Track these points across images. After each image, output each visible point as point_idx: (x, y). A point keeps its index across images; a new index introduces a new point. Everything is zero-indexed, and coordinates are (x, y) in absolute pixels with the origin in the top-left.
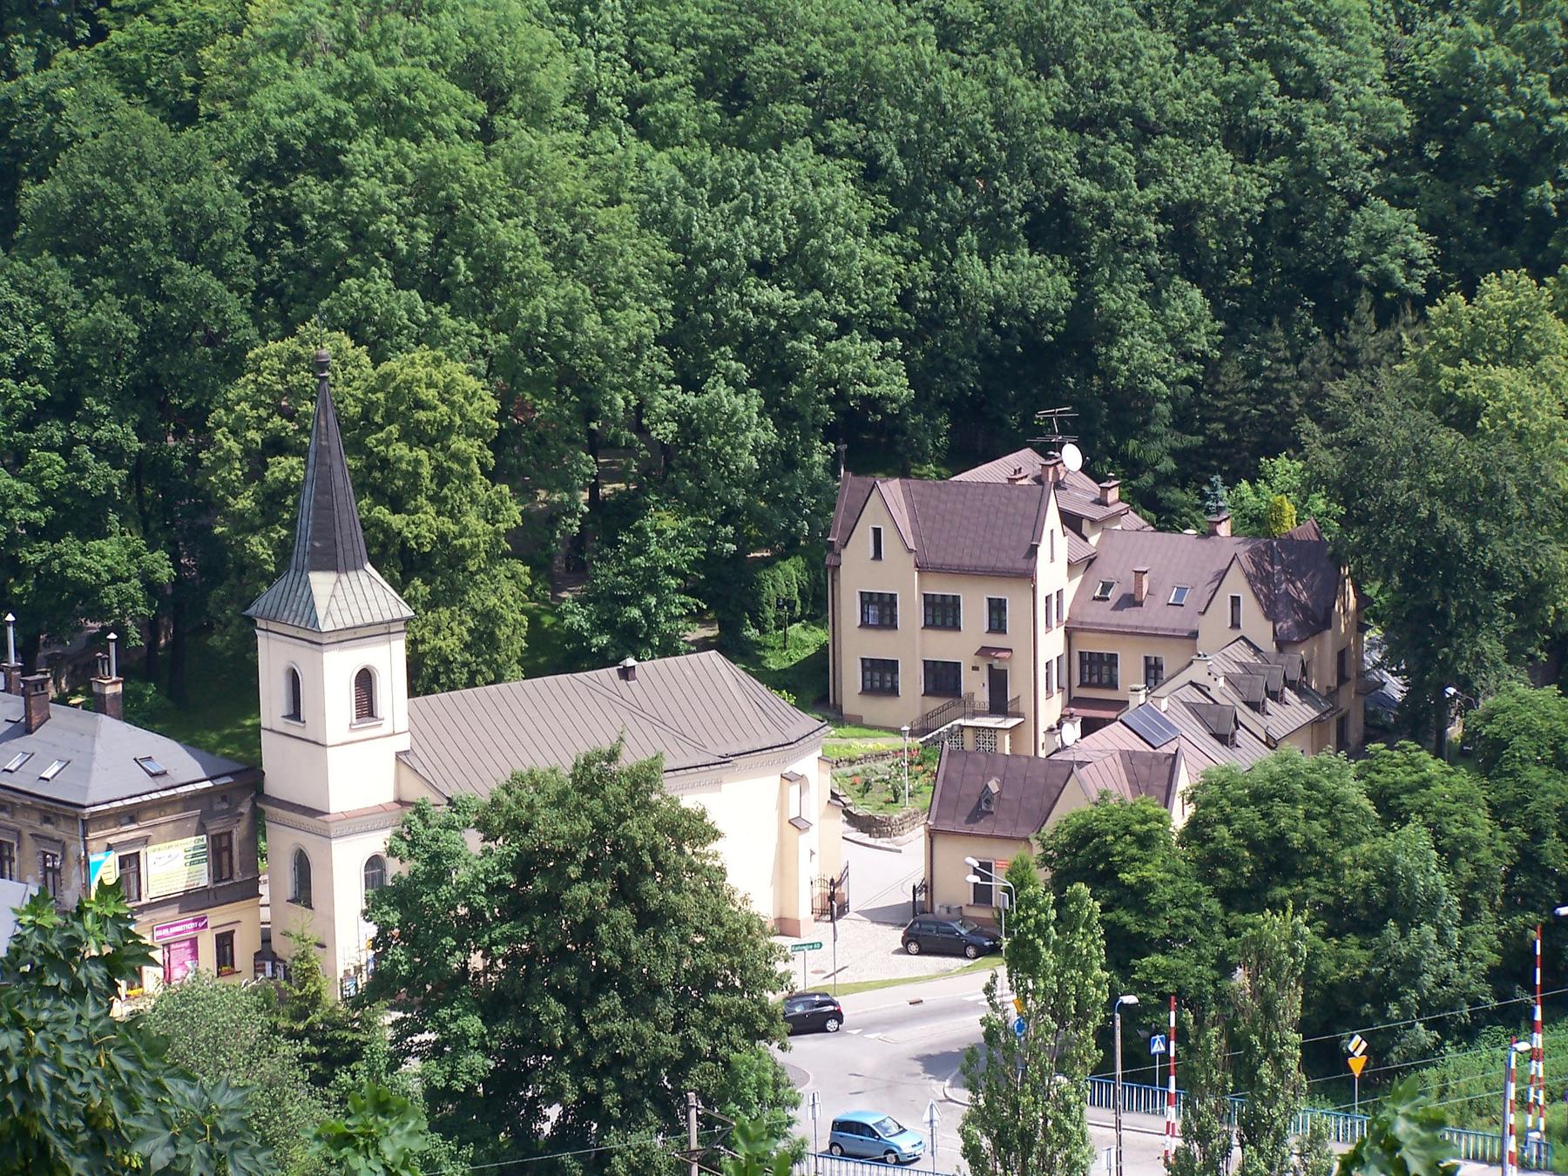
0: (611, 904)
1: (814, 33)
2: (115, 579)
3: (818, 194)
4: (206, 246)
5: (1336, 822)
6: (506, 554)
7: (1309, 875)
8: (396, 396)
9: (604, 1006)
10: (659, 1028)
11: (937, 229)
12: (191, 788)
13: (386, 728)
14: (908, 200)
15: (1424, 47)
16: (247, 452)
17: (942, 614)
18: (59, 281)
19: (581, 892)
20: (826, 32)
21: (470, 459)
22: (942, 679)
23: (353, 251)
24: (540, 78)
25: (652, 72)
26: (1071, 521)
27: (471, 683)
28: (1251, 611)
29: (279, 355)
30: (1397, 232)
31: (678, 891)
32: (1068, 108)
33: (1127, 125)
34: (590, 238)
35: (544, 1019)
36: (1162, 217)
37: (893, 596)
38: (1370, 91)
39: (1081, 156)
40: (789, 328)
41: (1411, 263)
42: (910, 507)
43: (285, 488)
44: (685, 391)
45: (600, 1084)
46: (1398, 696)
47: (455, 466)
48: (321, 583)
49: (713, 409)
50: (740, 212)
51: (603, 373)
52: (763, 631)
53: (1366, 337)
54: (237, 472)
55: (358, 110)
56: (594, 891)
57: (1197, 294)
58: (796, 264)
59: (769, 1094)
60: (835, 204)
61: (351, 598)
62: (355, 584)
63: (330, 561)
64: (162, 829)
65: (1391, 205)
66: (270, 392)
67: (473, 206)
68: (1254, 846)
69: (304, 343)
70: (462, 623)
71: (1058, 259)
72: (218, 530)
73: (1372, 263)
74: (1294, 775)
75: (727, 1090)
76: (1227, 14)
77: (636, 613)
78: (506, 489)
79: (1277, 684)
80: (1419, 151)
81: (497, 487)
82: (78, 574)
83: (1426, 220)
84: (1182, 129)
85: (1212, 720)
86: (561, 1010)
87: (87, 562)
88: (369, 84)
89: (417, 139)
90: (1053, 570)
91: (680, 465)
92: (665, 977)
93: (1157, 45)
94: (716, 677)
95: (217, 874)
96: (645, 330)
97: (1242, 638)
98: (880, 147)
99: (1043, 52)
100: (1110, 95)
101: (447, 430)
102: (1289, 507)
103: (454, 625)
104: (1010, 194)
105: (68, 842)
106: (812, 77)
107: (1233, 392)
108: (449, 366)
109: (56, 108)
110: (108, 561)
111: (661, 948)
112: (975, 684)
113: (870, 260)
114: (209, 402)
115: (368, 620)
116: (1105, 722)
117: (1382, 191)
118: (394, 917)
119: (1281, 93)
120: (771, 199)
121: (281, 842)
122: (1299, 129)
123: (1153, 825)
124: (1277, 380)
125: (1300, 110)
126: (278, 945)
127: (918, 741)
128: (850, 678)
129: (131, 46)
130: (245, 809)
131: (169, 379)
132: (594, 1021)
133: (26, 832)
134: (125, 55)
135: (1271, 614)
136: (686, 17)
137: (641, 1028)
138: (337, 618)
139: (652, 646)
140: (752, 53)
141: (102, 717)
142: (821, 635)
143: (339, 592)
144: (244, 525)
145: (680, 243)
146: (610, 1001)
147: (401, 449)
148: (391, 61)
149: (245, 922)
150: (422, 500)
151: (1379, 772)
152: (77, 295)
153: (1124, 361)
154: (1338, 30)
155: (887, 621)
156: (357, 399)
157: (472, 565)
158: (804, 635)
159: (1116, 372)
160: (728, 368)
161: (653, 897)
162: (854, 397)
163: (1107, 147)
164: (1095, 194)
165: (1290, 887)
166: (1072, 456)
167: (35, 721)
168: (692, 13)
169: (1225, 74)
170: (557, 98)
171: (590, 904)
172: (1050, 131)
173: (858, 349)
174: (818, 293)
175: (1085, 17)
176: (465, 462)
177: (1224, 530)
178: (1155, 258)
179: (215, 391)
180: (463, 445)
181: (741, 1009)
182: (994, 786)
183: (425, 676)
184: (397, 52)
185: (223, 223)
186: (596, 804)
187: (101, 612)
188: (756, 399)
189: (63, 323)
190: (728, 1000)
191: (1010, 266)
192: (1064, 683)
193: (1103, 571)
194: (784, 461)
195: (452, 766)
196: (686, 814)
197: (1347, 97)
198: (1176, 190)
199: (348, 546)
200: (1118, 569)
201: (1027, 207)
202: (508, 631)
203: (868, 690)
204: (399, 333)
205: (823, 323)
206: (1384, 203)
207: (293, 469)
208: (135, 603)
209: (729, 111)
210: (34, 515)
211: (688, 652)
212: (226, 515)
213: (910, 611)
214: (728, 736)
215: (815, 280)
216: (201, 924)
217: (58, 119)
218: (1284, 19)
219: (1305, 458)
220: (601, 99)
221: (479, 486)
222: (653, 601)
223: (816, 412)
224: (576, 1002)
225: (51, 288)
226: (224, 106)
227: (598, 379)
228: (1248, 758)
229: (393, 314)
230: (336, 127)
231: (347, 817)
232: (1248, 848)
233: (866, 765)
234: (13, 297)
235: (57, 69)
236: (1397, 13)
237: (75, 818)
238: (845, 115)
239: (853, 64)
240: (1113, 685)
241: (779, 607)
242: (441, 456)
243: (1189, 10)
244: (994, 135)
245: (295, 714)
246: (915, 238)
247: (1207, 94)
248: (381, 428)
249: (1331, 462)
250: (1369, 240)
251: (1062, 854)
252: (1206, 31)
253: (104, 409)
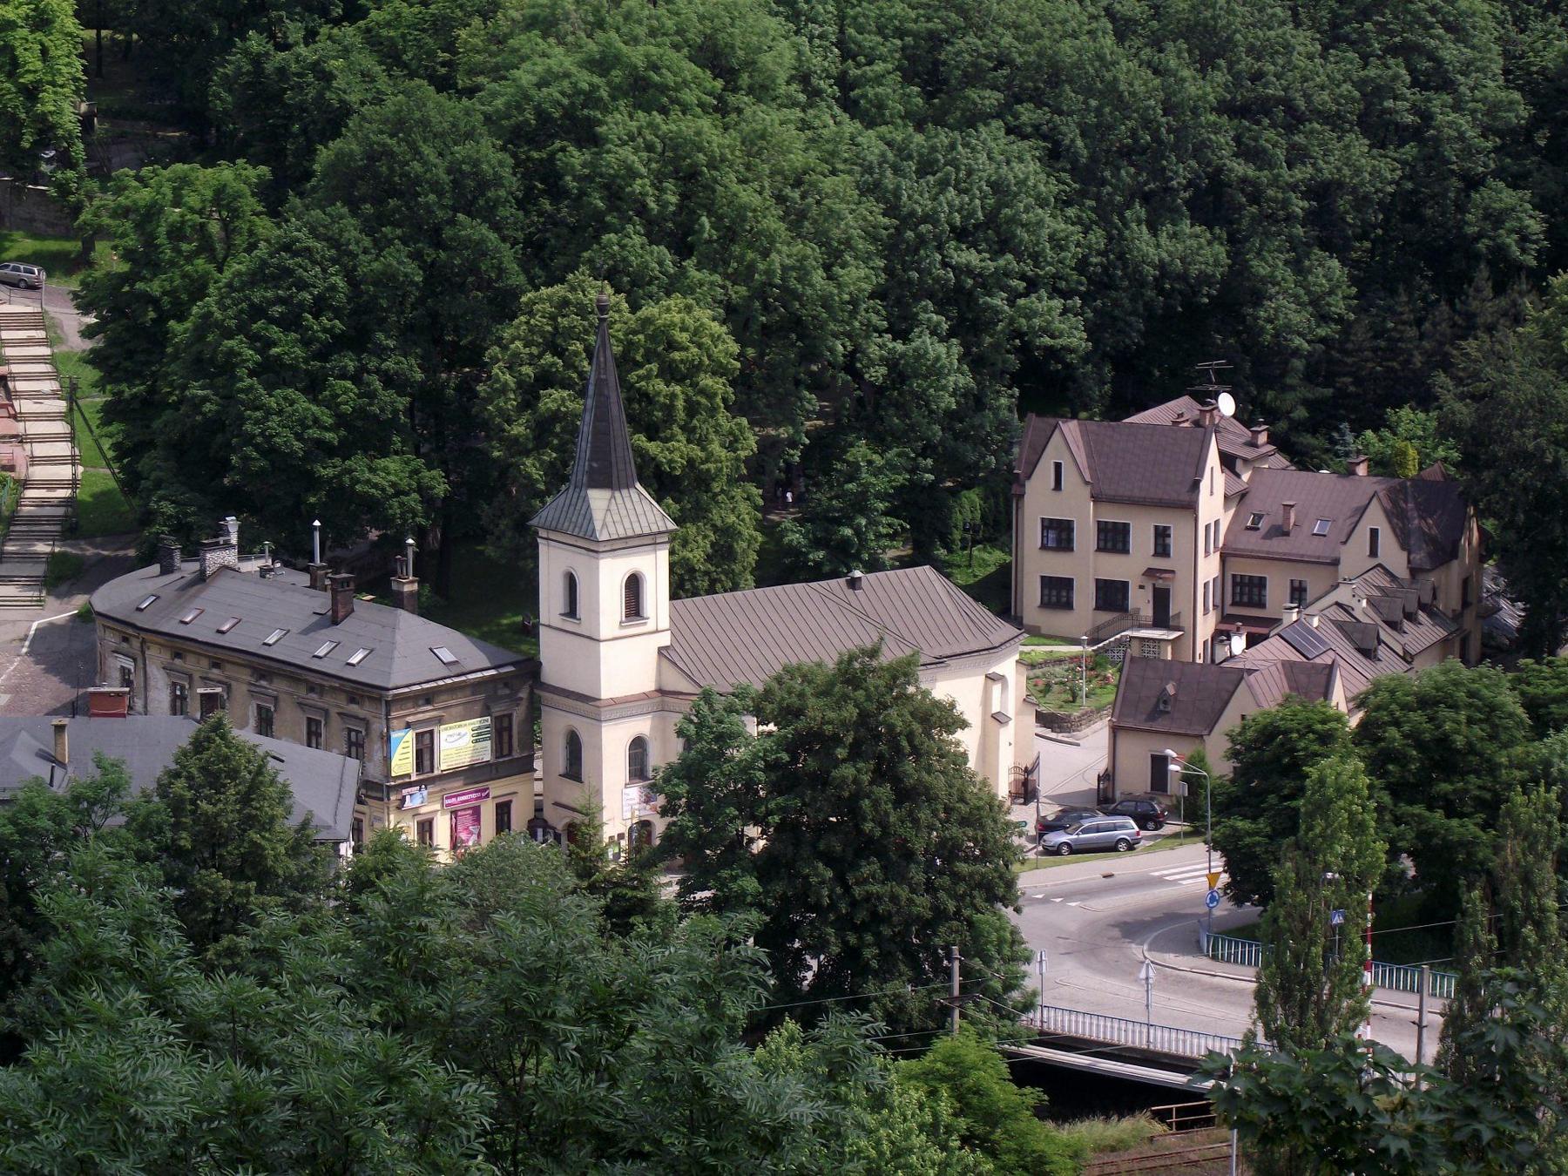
0: (871, 783)
1: (1006, 26)
2: (398, 493)
3: (1012, 169)
4: (481, 202)
5: (1494, 726)
6: (742, 478)
7: (1469, 773)
8: (652, 338)
9: (865, 871)
10: (913, 891)
11: (1111, 201)
12: (479, 675)
13: (651, 626)
14: (1087, 176)
15: (1539, 45)
16: (520, 384)
18: (351, 230)
19: (848, 771)
20: (1017, 26)
21: (716, 394)
22: (1111, 595)
23: (610, 210)
24: (766, 59)
25: (862, 59)
26: (1228, 461)
27: (711, 591)
28: (1387, 540)
29: (549, 299)
30: (1513, 210)
31: (929, 771)
32: (1229, 97)
33: (1279, 112)
34: (818, 203)
35: (813, 880)
36: (1305, 196)
38: (1491, 84)
39: (1238, 139)
40: (983, 286)
41: (1524, 238)
42: (1087, 444)
43: (555, 416)
44: (894, 340)
45: (860, 938)
46: (1513, 622)
47: (703, 401)
48: (598, 499)
49: (920, 355)
50: (943, 184)
51: (826, 322)
52: (950, 551)
53: (1484, 303)
54: (511, 402)
55: (609, 84)
56: (859, 771)
57: (1335, 263)
58: (994, 231)
59: (1006, 951)
60: (1027, 178)
61: (623, 512)
62: (627, 500)
63: (605, 479)
64: (453, 711)
65: (1508, 186)
66: (542, 334)
67: (715, 173)
68: (1420, 745)
69: (573, 289)
70: (705, 537)
71: (1217, 231)
72: (496, 454)
73: (1490, 238)
74: (1456, 684)
75: (976, 947)
76: (1365, 15)
77: (848, 532)
78: (744, 421)
79: (1412, 606)
80: (1529, 139)
81: (738, 420)
82: (366, 488)
83: (1537, 200)
84: (1333, 120)
85: (1356, 636)
86: (829, 874)
87: (376, 479)
88: (617, 59)
89: (664, 111)
90: (1212, 504)
91: (878, 407)
92: (919, 846)
93: (1304, 41)
94: (930, 589)
95: (499, 750)
96: (864, 286)
97: (1380, 565)
98: (1064, 129)
99: (1209, 47)
100: (1266, 86)
101: (696, 368)
102: (1412, 452)
103: (699, 539)
104: (1176, 173)
105: (372, 720)
106: (1000, 64)
107: (1361, 350)
108: (697, 312)
109: (327, 77)
110: (392, 478)
111: (916, 821)
112: (1140, 601)
113: (1055, 229)
114: (484, 339)
115: (638, 531)
116: (1266, 637)
117: (1498, 174)
118: (683, 789)
119: (1413, 85)
120: (970, 173)
121: (555, 725)
122: (1427, 117)
123: (1333, 725)
124: (1400, 340)
125: (1429, 100)
126: (550, 814)
127: (1090, 649)
128: (1031, 593)
129: (388, 24)
130: (524, 694)
131: (449, 319)
132: (857, 883)
133: (333, 711)
134: (384, 32)
135: (1405, 545)
136: (893, 12)
137: (897, 889)
138: (612, 530)
139: (861, 561)
140: (952, 44)
141: (401, 611)
142: (994, 557)
143: (613, 507)
144: (516, 447)
145: (892, 210)
146: (871, 867)
147: (660, 385)
148: (635, 40)
149: (522, 793)
150: (676, 428)
151: (1529, 684)
152: (367, 242)
153: (1270, 321)
154: (1464, 29)
155: (1120, 546)
156: (619, 340)
157: (716, 487)
158: (986, 556)
159: (1262, 330)
160: (929, 320)
161: (910, 776)
162: (1038, 348)
163: (1260, 132)
164: (1250, 173)
165: (1452, 783)
166: (1226, 404)
167: (341, 614)
168: (899, 8)
169: (1364, 68)
170: (781, 80)
171: (856, 781)
172: (1213, 118)
173: (1045, 305)
174: (1009, 256)
175: (1244, 17)
176: (711, 396)
177: (1362, 470)
178: (1299, 231)
179: (489, 331)
180: (709, 382)
181: (983, 876)
182: (1170, 689)
183: (683, 584)
184: (641, 31)
185: (498, 182)
186: (860, 694)
187: (383, 521)
188: (956, 349)
189: (355, 268)
190: (972, 868)
191: (1174, 236)
192: (1218, 602)
193: (1255, 504)
194: (975, 401)
195: (707, 662)
196: (937, 704)
197: (1472, 89)
198: (1320, 170)
199: (621, 466)
200: (1267, 504)
201: (1190, 184)
202: (745, 545)
203: (1046, 604)
204: (650, 283)
205: (1015, 283)
206: (1502, 185)
207: (563, 399)
208: (415, 515)
209: (929, 96)
210: (329, 436)
211: (893, 568)
212: (500, 440)
213: (1086, 536)
214: (941, 639)
215: (1004, 244)
216: (484, 794)
217: (329, 87)
218: (1418, 19)
219: (1440, 408)
220: (815, 81)
221: (722, 417)
222: (864, 522)
223: (1004, 362)
224: (841, 867)
225: (346, 235)
226: (481, 79)
227: (821, 327)
228: (1389, 666)
229: (646, 267)
230: (591, 99)
231: (615, 702)
232: (1415, 748)
233: (1045, 669)
234: (311, 243)
235: (323, 44)
236: (1513, 15)
237: (378, 700)
238: (1031, 99)
239: (1040, 54)
240: (1262, 605)
241: (965, 530)
242: (690, 391)
243: (1332, 11)
244: (1164, 120)
245: (572, 612)
246: (1093, 209)
247: (1347, 87)
248: (639, 365)
249: (1464, 412)
250: (1487, 216)
251: (1249, 749)
252: (1347, 28)
253: (391, 343)
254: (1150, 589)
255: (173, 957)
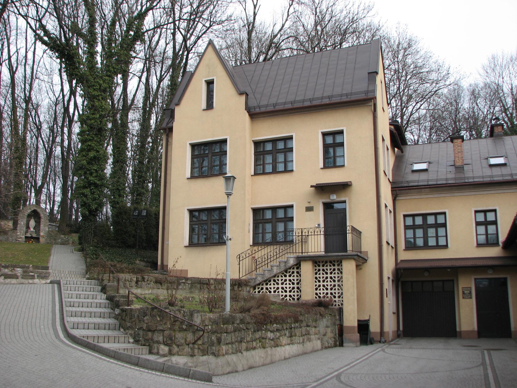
17: (272, 156)
37: (194, 146)
213: (240, 158)
254: (320, 210)
255: (468, 152)
